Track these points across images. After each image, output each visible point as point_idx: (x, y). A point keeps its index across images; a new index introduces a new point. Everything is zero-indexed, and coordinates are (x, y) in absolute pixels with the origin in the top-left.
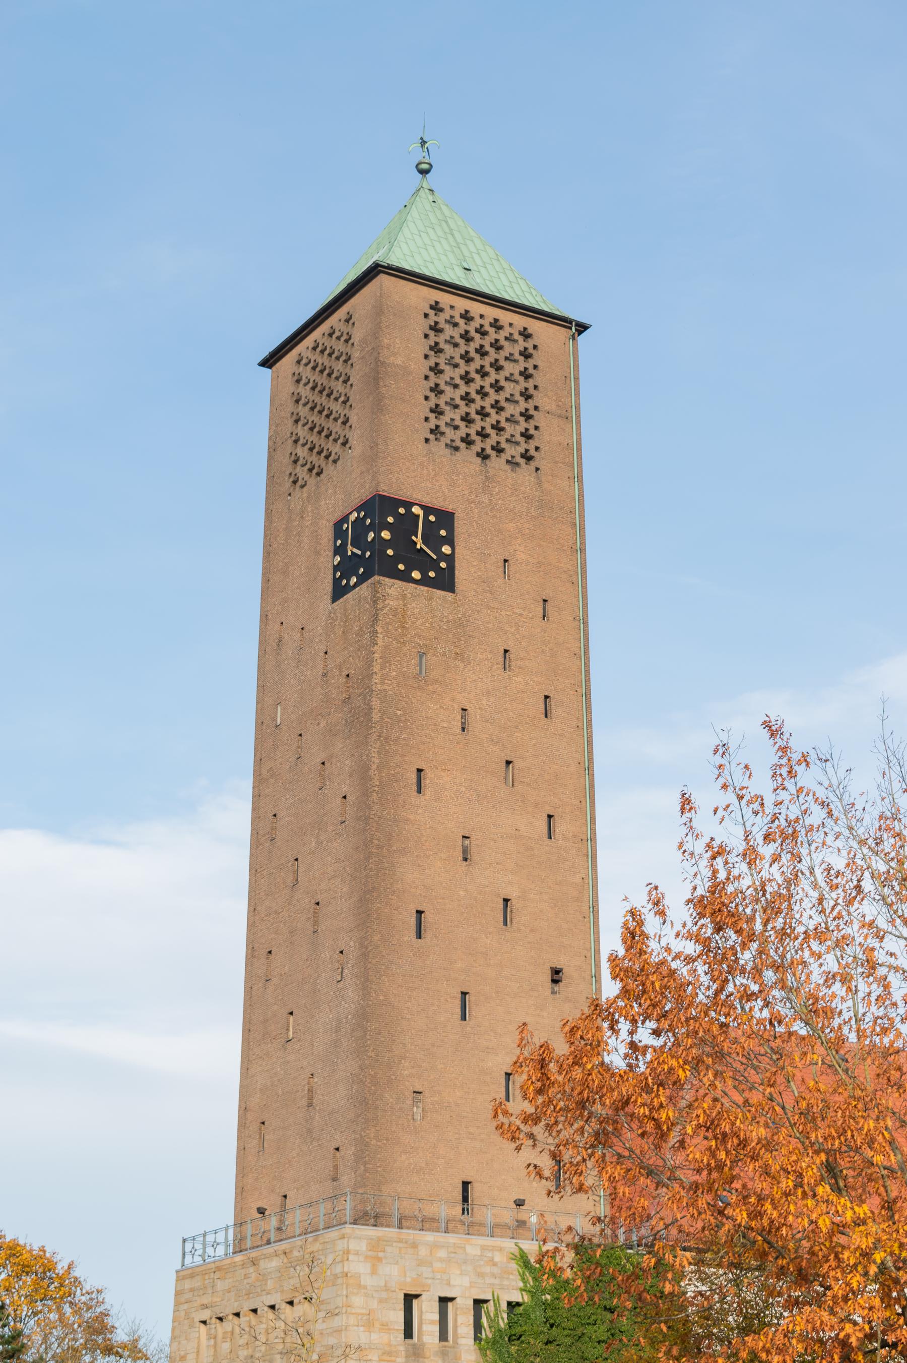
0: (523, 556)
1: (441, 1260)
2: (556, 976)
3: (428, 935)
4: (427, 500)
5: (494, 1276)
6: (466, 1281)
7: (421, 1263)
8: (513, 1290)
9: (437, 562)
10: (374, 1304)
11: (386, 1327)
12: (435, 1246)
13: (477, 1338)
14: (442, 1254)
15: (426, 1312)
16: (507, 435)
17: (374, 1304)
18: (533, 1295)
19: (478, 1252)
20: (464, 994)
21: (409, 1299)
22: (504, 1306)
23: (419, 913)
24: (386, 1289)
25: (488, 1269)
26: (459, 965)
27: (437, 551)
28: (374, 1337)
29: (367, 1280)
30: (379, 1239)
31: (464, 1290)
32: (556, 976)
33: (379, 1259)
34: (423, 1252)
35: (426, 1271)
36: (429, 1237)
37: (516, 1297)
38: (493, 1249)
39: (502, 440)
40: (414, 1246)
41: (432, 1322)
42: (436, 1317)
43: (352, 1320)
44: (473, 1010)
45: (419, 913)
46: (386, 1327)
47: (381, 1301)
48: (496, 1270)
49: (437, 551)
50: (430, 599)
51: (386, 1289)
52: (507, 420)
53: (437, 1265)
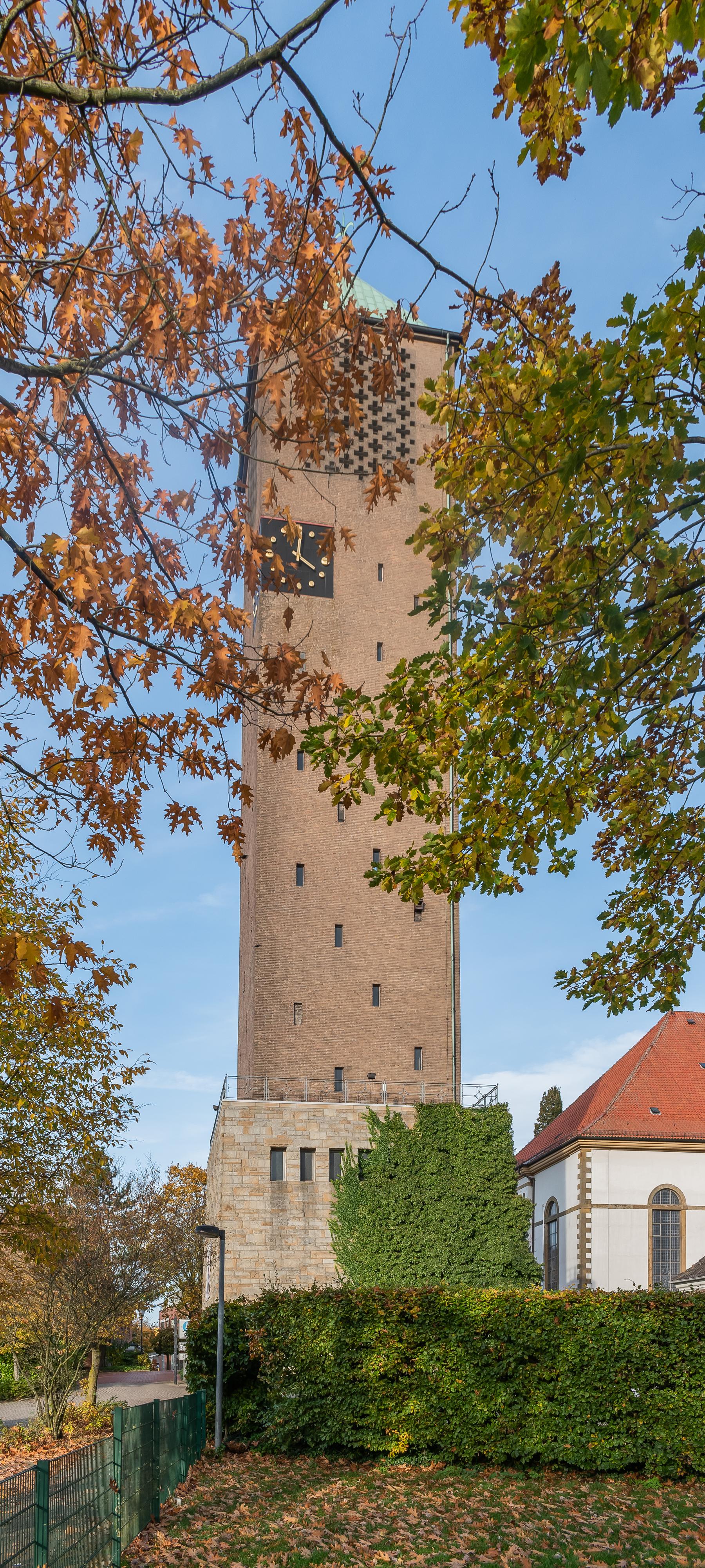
0: (396, 559)
1: (302, 1121)
2: (95, 904)
3: (307, 883)
4: (307, 519)
5: (347, 1131)
6: (323, 1136)
7: (285, 1124)
8: (362, 1140)
9: (315, 572)
10: (246, 1155)
11: (255, 1171)
12: (298, 1111)
13: (332, 1177)
14: (304, 1117)
15: (291, 1162)
16: (384, 452)
17: (246, 1155)
18: (379, 1143)
19: (334, 1114)
20: (338, 927)
21: (277, 1151)
22: (355, 1152)
23: (300, 866)
24: (256, 1144)
25: (342, 1126)
26: (334, 904)
27: (317, 562)
28: (246, 1179)
29: (240, 1139)
30: (250, 1109)
31: (321, 1141)
32: (95, 904)
33: (251, 1123)
34: (287, 1116)
35: (290, 1130)
36: (294, 1104)
37: (366, 1145)
38: (347, 1111)
39: (379, 456)
40: (280, 1112)
41: (294, 1167)
42: (298, 1162)
43: (227, 1168)
44: (345, 937)
45: (300, 866)
46: (255, 1171)
47: (251, 1153)
48: (349, 1127)
49: (317, 562)
50: (309, 605)
51: (256, 1144)
52: (384, 438)
53: (299, 1125)
